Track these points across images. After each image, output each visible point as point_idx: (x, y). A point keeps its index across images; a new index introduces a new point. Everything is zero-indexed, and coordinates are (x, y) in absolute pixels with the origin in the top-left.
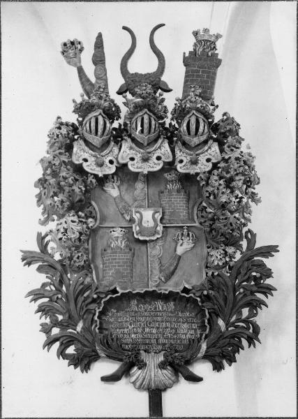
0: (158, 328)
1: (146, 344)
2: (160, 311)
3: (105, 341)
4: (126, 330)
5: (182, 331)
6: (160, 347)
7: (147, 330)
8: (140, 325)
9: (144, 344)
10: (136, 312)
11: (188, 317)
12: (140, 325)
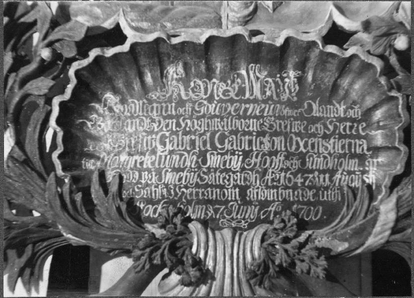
0: (246, 154)
1: (209, 202)
2: (255, 101)
3: (78, 197)
4: (148, 160)
5: (317, 162)
6: (252, 212)
7: (214, 160)
8: (193, 143)
9: (199, 202)
10: (181, 103)
11: (340, 120)
12: (193, 143)
